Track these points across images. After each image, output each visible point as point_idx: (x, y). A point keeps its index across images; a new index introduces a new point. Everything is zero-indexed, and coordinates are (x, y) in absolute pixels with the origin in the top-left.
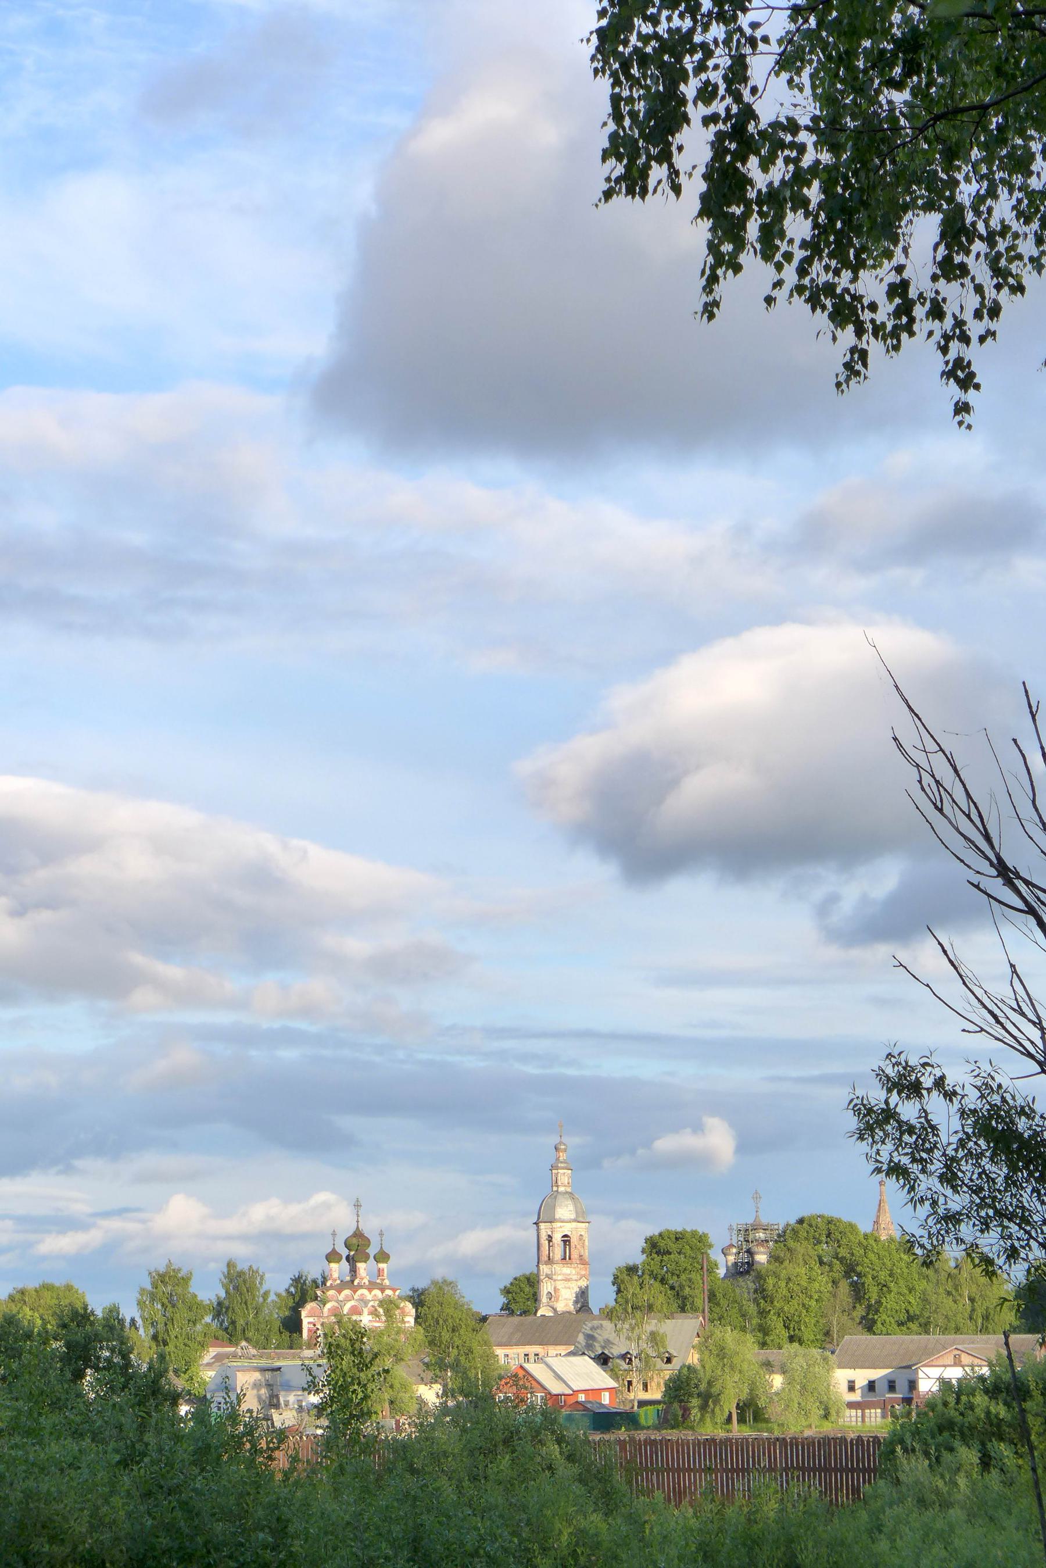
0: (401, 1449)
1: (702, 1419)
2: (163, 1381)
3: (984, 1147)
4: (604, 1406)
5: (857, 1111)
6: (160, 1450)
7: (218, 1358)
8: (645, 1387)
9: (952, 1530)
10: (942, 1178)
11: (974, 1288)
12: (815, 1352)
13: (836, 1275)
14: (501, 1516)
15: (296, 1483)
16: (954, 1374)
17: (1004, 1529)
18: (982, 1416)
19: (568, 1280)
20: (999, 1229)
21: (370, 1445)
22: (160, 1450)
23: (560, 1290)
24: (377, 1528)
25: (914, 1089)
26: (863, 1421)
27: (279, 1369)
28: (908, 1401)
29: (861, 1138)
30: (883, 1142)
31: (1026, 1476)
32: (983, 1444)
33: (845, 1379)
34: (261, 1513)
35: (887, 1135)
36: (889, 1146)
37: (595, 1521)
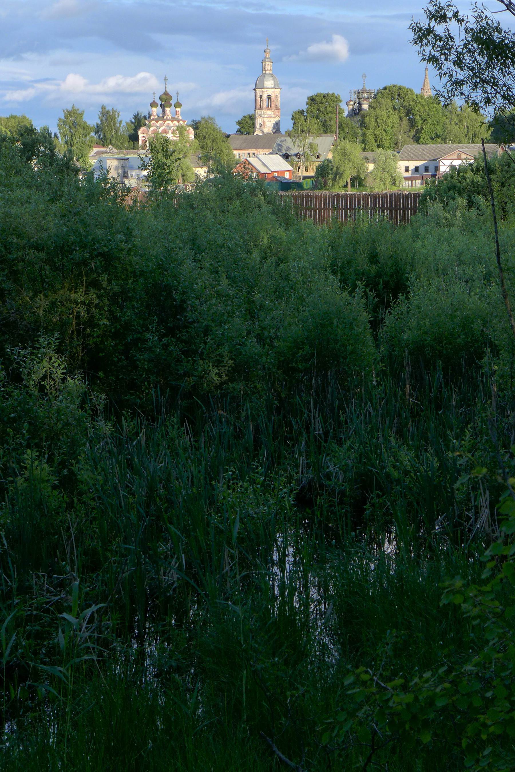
0: (187, 197)
1: (333, 185)
2: (71, 163)
3: (476, 47)
4: (286, 179)
5: (414, 30)
6: (70, 194)
7: (98, 153)
8: (307, 170)
9: (452, 237)
10: (455, 63)
11: (469, 122)
12: (390, 153)
13: (402, 115)
14: (235, 229)
15: (136, 212)
16: (457, 163)
17: (478, 237)
18: (470, 182)
19: (269, 117)
20: (482, 88)
21: (172, 196)
22: (70, 194)
23: (266, 122)
24: (176, 234)
25: (443, 18)
26: (412, 186)
27: (127, 159)
28: (434, 176)
29: (416, 43)
30: (427, 45)
31: (489, 211)
32: (470, 196)
33: (404, 166)
34: (119, 225)
35: (429, 42)
36: (430, 47)
37: (280, 232)
